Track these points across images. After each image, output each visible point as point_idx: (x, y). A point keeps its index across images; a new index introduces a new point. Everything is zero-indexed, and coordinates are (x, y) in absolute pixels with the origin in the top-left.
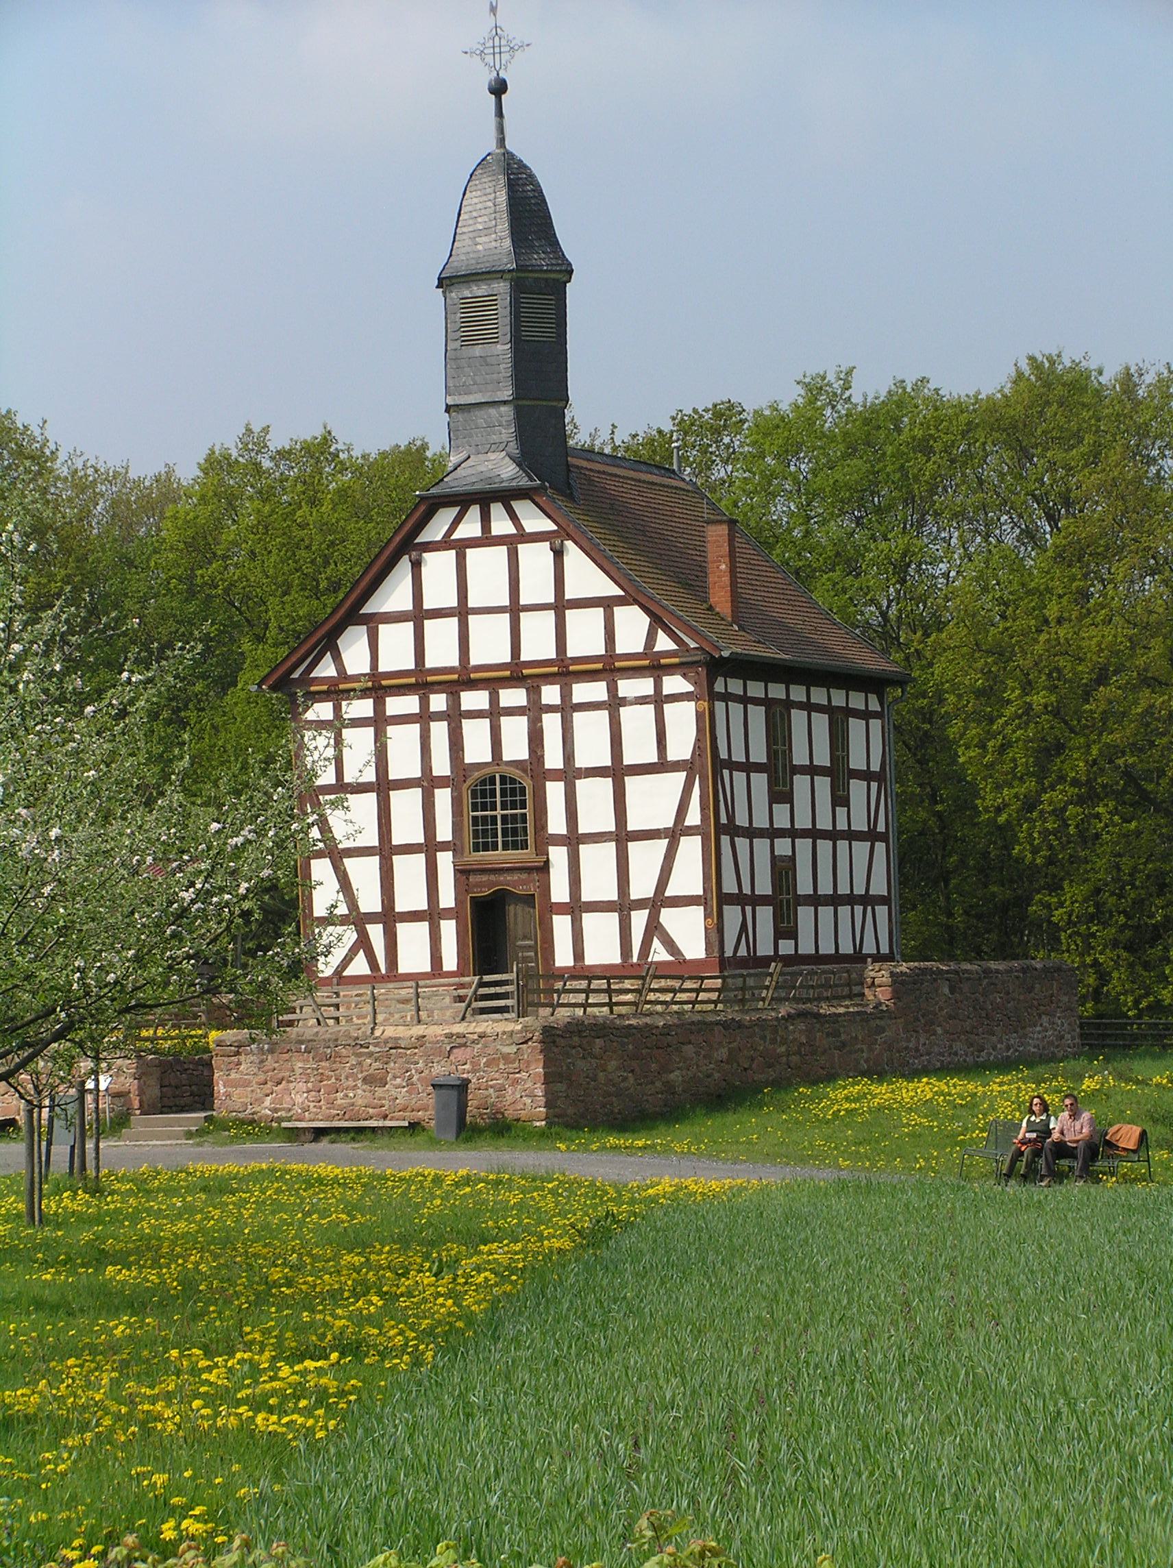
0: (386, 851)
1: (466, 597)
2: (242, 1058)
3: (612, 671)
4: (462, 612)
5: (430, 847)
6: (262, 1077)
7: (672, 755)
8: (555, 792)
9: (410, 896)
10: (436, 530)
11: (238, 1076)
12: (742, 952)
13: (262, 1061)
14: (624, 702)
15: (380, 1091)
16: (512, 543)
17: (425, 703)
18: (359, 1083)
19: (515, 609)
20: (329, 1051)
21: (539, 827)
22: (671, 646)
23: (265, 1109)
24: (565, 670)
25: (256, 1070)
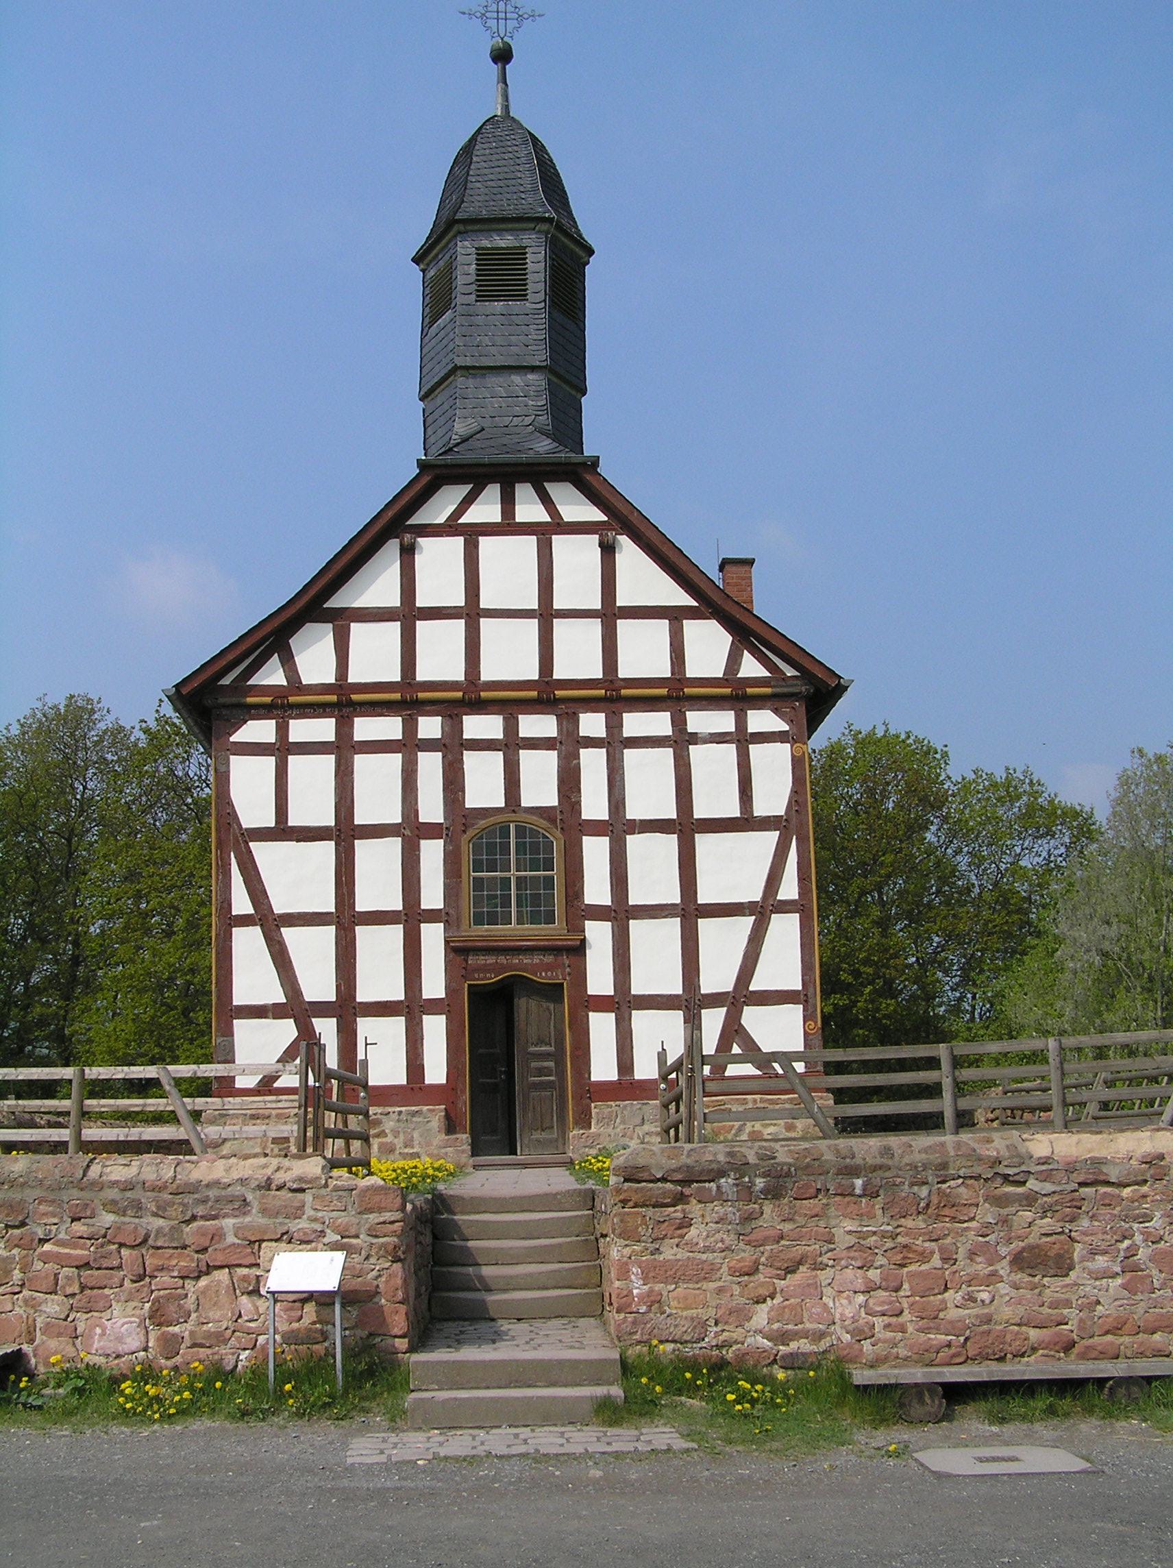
0: (346, 919)
1: (478, 596)
2: (694, 1208)
3: (678, 698)
4: (472, 613)
5: (411, 917)
6: (746, 1255)
7: (761, 809)
8: (595, 851)
9: (380, 975)
10: (439, 509)
11: (682, 1254)
13: (748, 1218)
14: (694, 739)
15: (1054, 1287)
16: (544, 533)
17: (410, 727)
18: (1003, 1268)
19: (546, 614)
20: (924, 1192)
21: (571, 893)
22: (760, 671)
23: (756, 1332)
24: (614, 694)
25: (730, 1239)
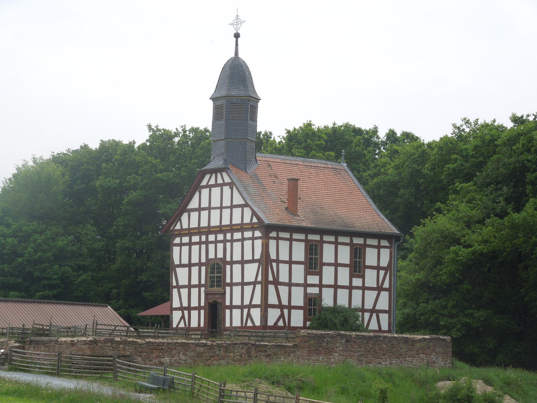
12: (182, 325)
